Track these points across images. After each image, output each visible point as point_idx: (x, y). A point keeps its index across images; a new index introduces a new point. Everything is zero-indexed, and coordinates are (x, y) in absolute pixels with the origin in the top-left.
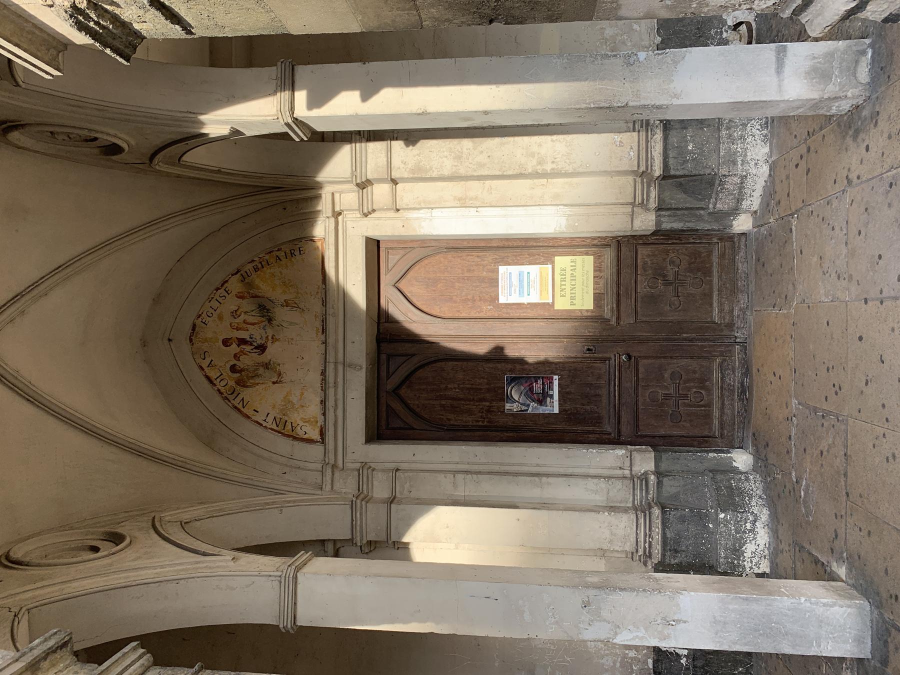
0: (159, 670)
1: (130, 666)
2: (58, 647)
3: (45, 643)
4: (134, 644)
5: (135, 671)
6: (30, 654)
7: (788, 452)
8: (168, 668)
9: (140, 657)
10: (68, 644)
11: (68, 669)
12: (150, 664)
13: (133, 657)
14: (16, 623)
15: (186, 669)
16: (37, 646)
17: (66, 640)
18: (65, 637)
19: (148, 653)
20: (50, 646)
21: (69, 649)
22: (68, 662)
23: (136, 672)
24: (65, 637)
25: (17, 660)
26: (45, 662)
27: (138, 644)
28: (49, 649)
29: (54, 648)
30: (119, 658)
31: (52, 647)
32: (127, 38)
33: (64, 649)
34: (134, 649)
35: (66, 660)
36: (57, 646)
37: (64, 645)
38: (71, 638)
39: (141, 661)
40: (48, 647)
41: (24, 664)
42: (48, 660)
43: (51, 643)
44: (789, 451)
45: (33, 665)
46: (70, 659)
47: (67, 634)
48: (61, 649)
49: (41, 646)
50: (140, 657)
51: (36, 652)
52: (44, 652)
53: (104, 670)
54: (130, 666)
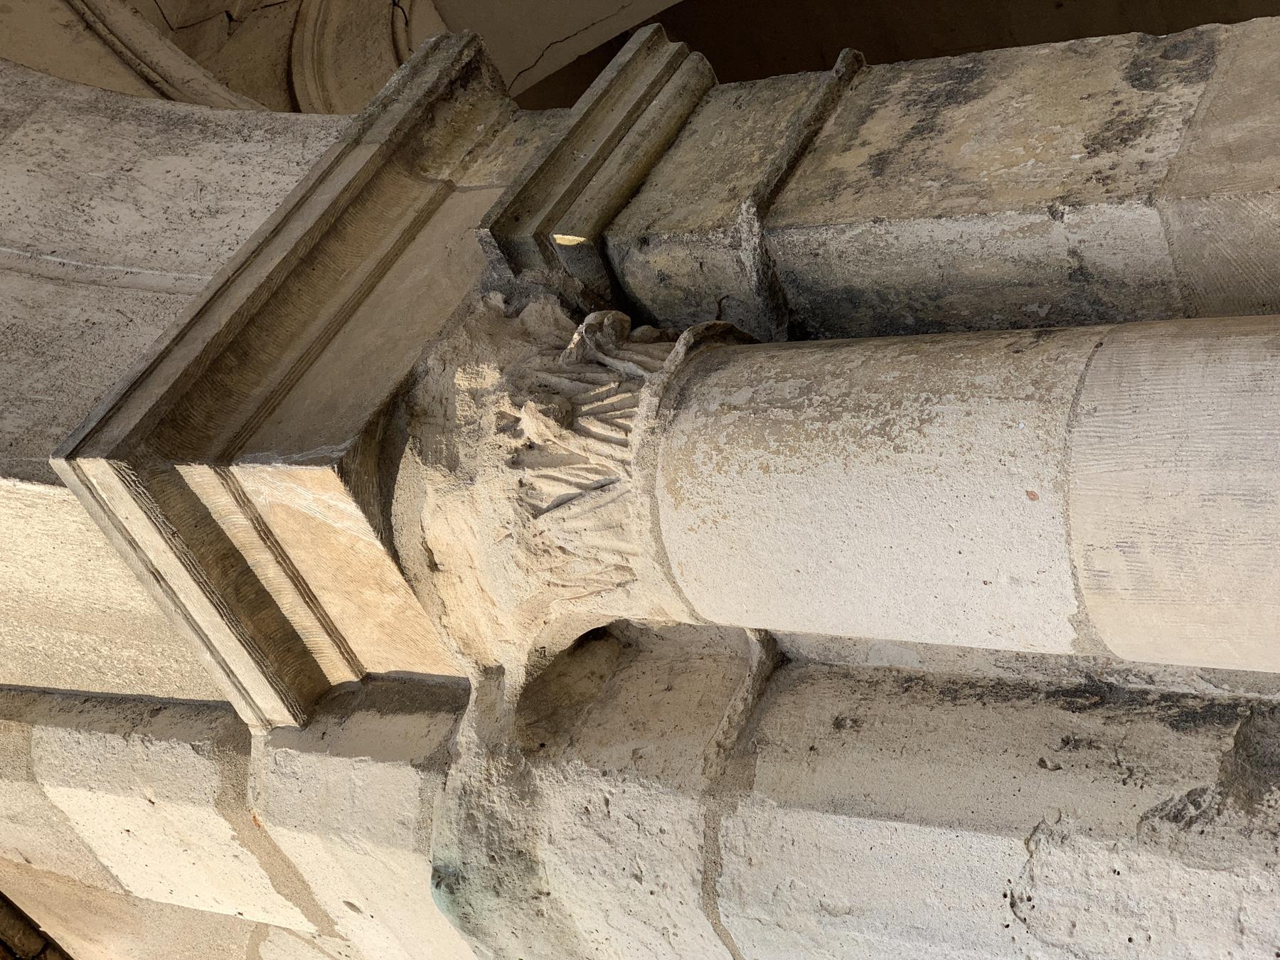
0: (735, 94)
1: (647, 98)
2: (452, 83)
3: (417, 80)
4: (645, 33)
5: (664, 110)
6: (386, 117)
7: (851, 224)
8: (761, 82)
9: (672, 67)
10: (478, 68)
11: (500, 135)
12: (707, 81)
13: (652, 69)
14: (400, 24)
15: (812, 75)
16: (398, 91)
17: (465, 59)
18: (461, 53)
19: (692, 49)
20: (429, 85)
21: (487, 82)
22: (494, 116)
23: (669, 113)
24: (461, 53)
25: (357, 142)
26: (433, 131)
27: (656, 32)
28: (430, 92)
29: (441, 89)
30: (612, 83)
31: (435, 86)
32: (1241, 716)
33: (474, 85)
34: (650, 47)
35: (488, 111)
36: (446, 81)
37: (468, 74)
38: (480, 51)
39: (677, 79)
40: (426, 87)
41: (374, 148)
42: (440, 123)
43: (430, 76)
44: (853, 226)
45: (401, 146)
46: (494, 109)
47: (463, 43)
48: (464, 87)
49: (407, 91)
50: (672, 67)
51: (399, 110)
52: (418, 105)
53: (578, 125)
54: (647, 98)
